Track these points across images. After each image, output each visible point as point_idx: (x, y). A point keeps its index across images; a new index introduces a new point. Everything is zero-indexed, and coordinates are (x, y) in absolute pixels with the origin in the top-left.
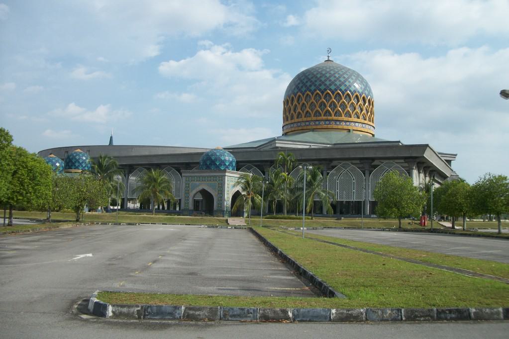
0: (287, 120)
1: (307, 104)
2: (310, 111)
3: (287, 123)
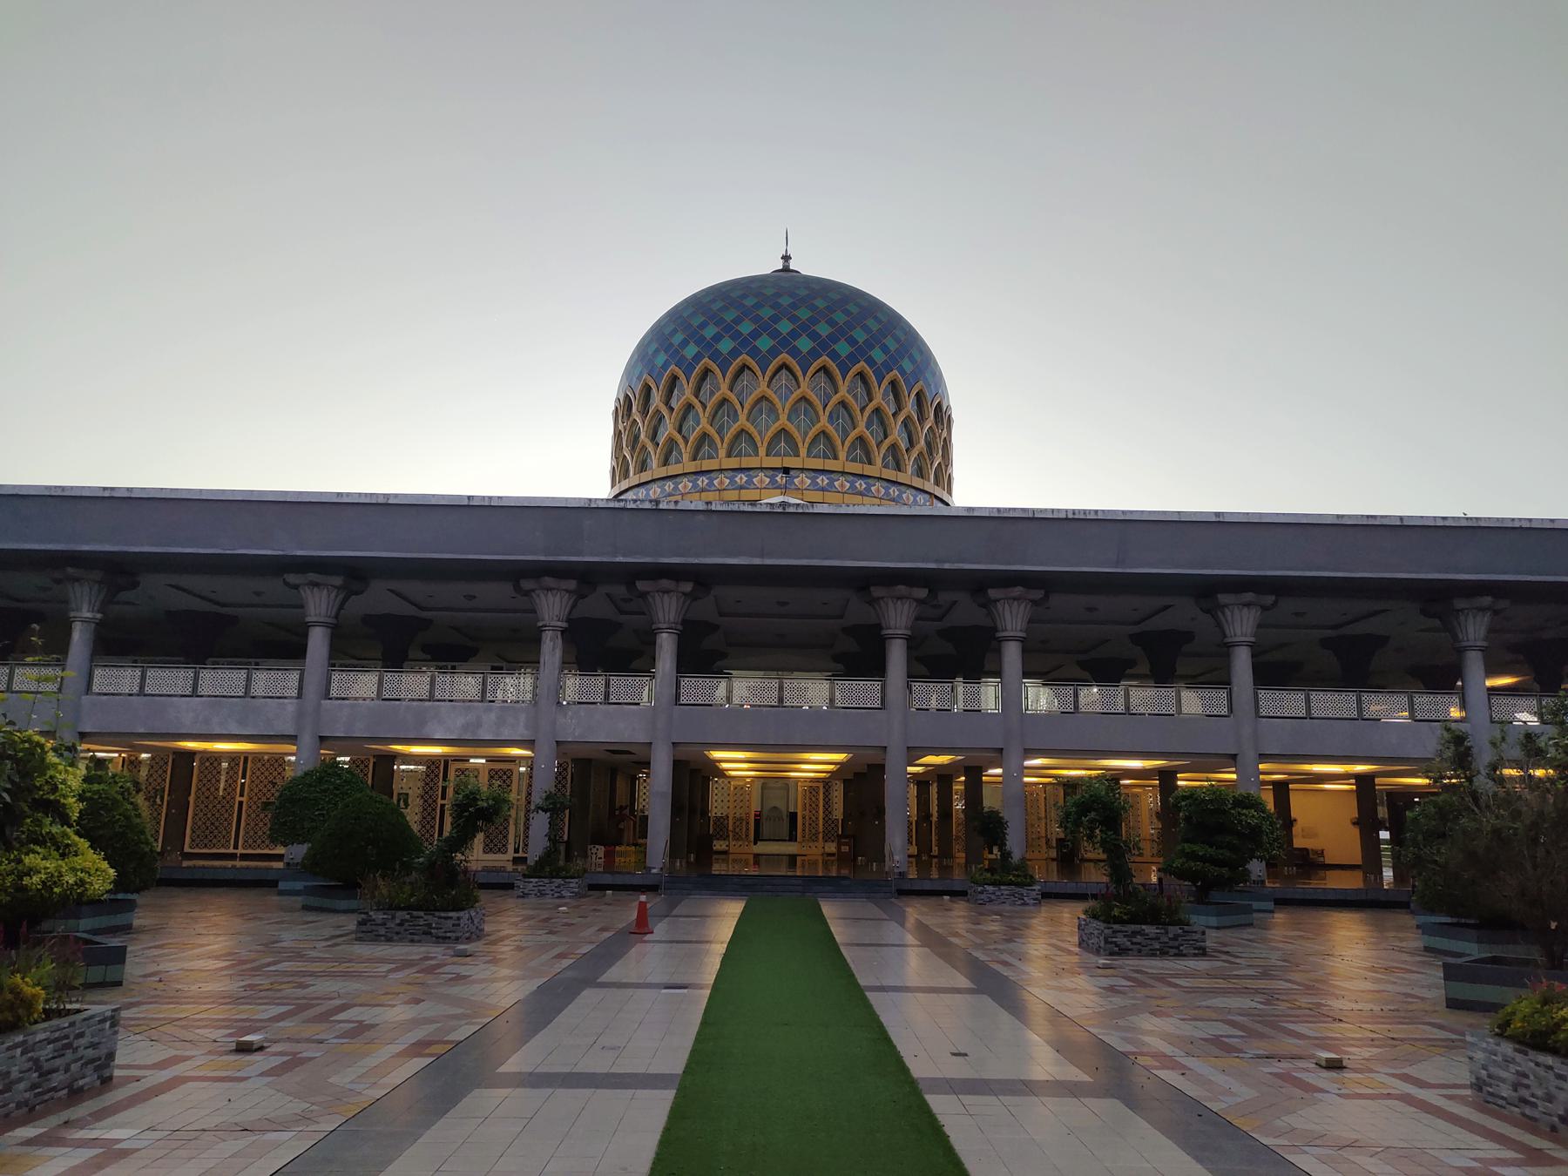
0: (626, 475)
1: (704, 406)
2: (712, 431)
3: (625, 485)
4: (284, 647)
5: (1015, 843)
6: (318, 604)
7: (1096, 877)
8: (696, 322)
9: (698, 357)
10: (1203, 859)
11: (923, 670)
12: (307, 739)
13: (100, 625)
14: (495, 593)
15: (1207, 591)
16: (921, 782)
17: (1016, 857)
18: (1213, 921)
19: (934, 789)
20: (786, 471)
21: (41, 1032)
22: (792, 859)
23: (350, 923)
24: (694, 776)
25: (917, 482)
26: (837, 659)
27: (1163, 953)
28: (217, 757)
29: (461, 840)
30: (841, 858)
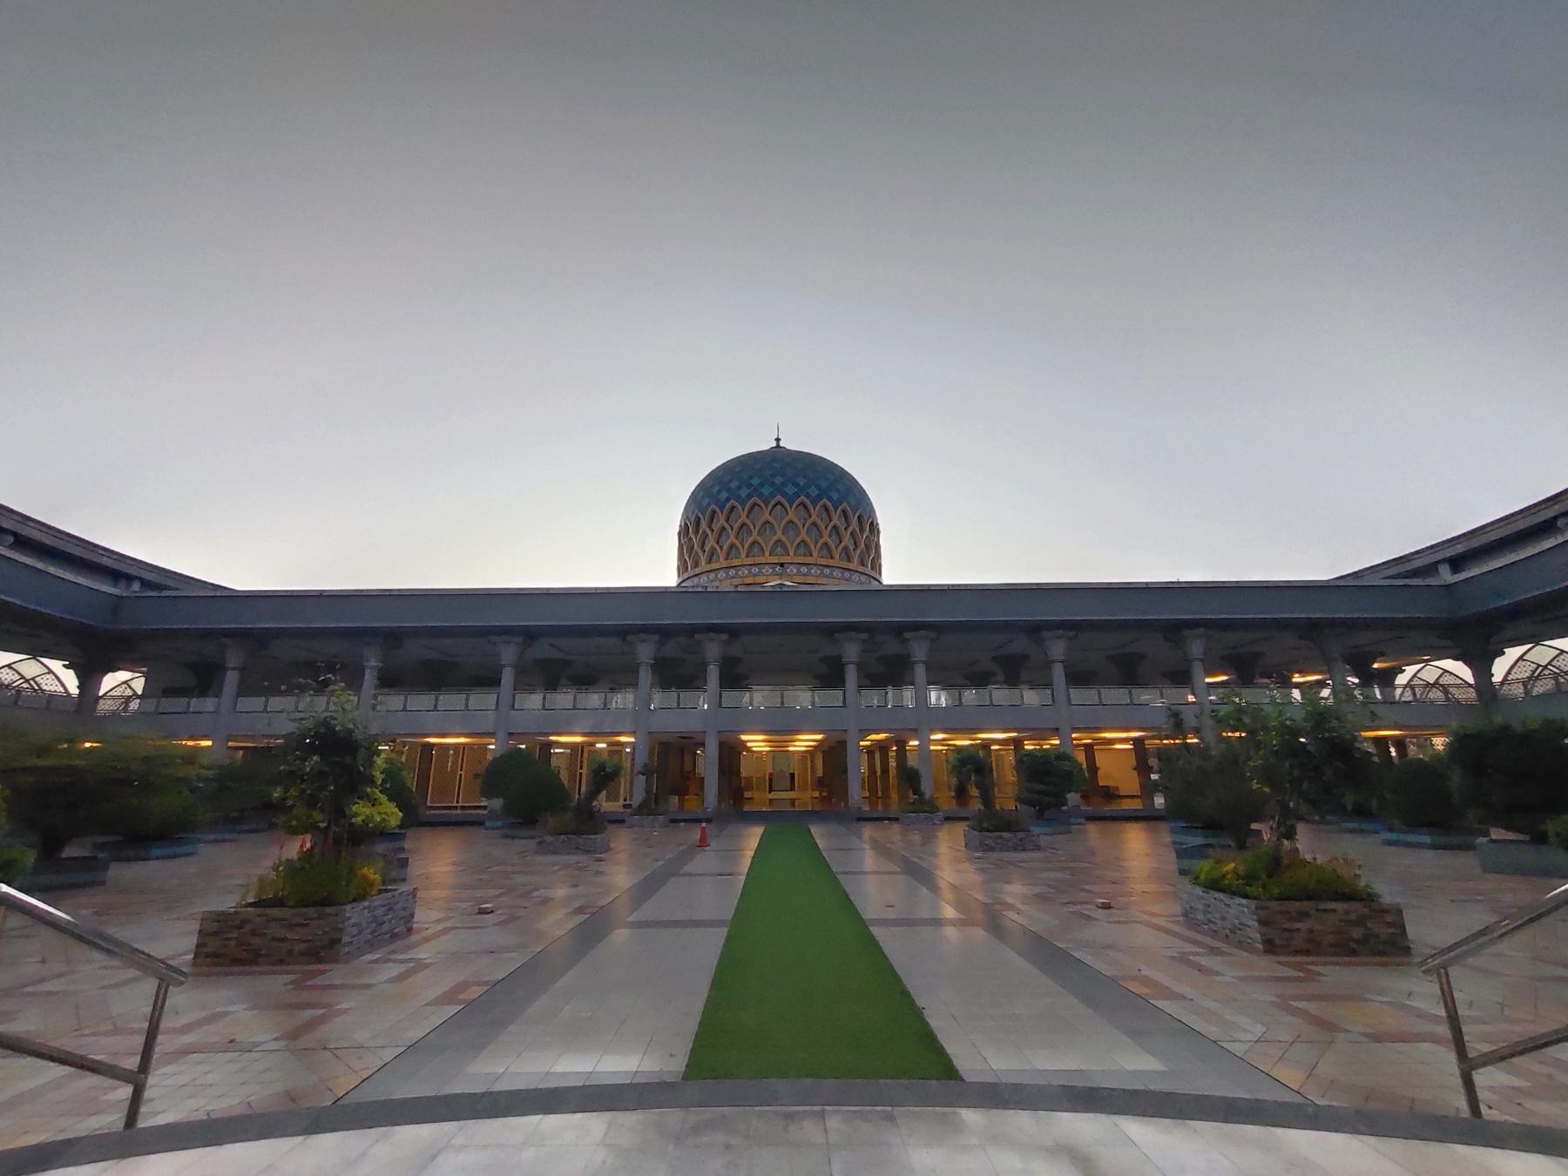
4: (490, 680)
5: (927, 787)
6: (508, 654)
7: (976, 806)
8: (726, 479)
9: (728, 500)
10: (1039, 792)
11: (867, 682)
12: (501, 735)
13: (380, 670)
14: (613, 643)
15: (1035, 630)
16: (870, 751)
17: (927, 796)
18: (1047, 830)
19: (877, 756)
20: (782, 565)
21: (378, 901)
22: (793, 802)
23: (532, 844)
24: (731, 753)
25: (861, 569)
26: (816, 677)
27: (1015, 849)
28: (446, 747)
29: (593, 794)
30: (822, 799)
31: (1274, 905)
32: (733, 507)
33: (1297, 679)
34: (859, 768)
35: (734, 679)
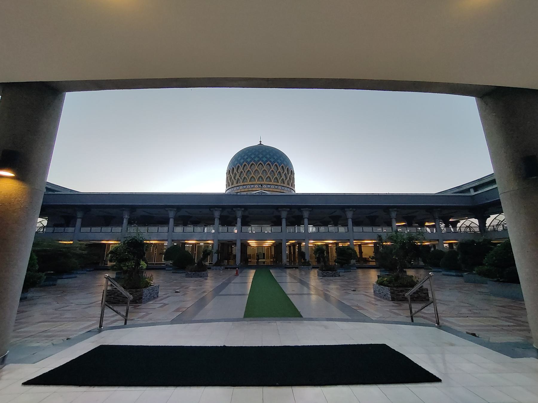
5: (307, 258)
6: (172, 214)
9: (243, 162)
11: (289, 224)
12: (170, 240)
15: (343, 208)
16: (290, 246)
17: (307, 261)
18: (343, 271)
19: (292, 248)
22: (264, 262)
23: (184, 275)
24: (245, 246)
25: (288, 186)
31: (395, 289)
32: (245, 165)
33: (427, 224)
34: (286, 252)
35: (246, 223)
